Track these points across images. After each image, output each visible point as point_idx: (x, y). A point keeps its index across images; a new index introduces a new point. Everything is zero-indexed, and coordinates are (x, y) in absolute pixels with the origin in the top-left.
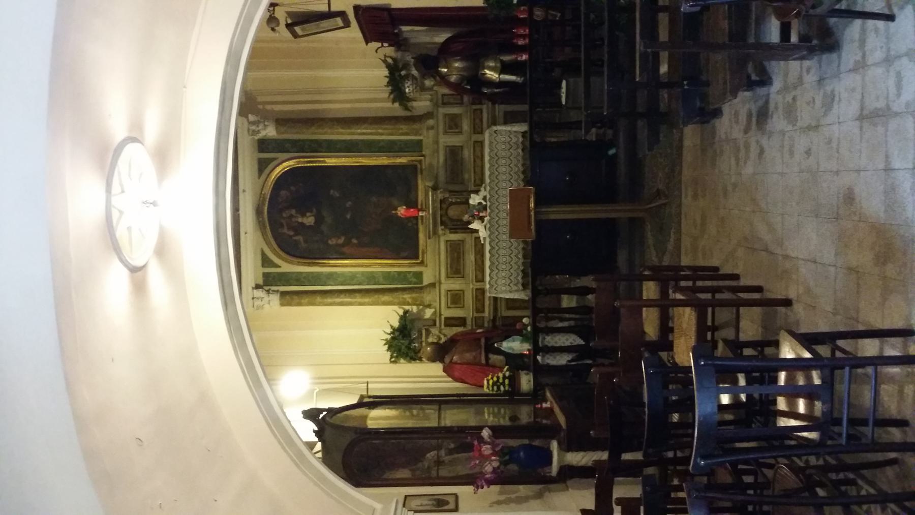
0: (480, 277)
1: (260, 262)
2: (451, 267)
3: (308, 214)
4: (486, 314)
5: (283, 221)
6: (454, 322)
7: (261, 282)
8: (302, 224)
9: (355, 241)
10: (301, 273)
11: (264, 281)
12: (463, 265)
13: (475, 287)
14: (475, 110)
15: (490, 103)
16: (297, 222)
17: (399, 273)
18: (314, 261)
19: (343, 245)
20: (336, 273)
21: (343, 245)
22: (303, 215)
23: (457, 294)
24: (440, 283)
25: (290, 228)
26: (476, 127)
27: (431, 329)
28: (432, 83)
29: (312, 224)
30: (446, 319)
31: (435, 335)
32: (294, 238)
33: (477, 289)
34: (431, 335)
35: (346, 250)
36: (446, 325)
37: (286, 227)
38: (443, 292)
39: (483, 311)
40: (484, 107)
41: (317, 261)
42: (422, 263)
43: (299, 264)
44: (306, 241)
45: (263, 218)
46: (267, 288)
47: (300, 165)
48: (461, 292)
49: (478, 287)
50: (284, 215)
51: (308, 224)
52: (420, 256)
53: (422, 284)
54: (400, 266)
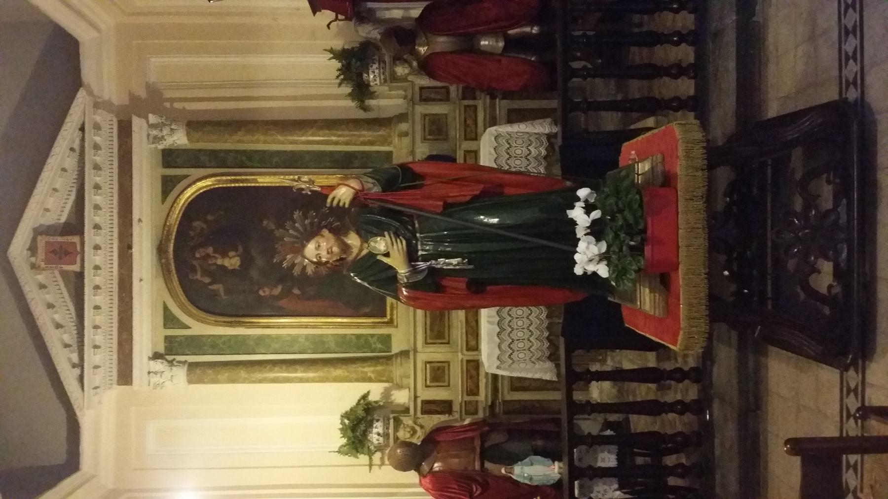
0: (473, 343)
1: (160, 320)
2: (432, 330)
3: (231, 254)
4: (482, 397)
5: (195, 263)
6: (433, 407)
7: (161, 349)
8: (223, 267)
9: (296, 291)
10: (220, 337)
11: (166, 347)
12: (449, 325)
13: (466, 358)
14: (466, 107)
15: (488, 97)
16: (215, 264)
17: (359, 337)
18: (238, 319)
19: (279, 297)
20: (269, 336)
21: (279, 297)
22: (224, 255)
23: (439, 368)
24: (415, 351)
25: (206, 272)
26: (468, 130)
27: (401, 418)
28: (407, 71)
29: (237, 267)
30: (426, 403)
31: (408, 425)
32: (210, 287)
33: (468, 361)
34: (402, 426)
35: (283, 303)
36: (424, 412)
37: (199, 273)
38: (420, 365)
39: (477, 393)
40: (480, 104)
41: (242, 320)
42: (390, 323)
43: (217, 324)
44: (228, 292)
45: (167, 259)
46: (170, 358)
47: (221, 186)
48: (446, 365)
49: (471, 358)
50: (198, 255)
51: (230, 268)
52: (388, 313)
53: (390, 352)
54: (358, 326)
